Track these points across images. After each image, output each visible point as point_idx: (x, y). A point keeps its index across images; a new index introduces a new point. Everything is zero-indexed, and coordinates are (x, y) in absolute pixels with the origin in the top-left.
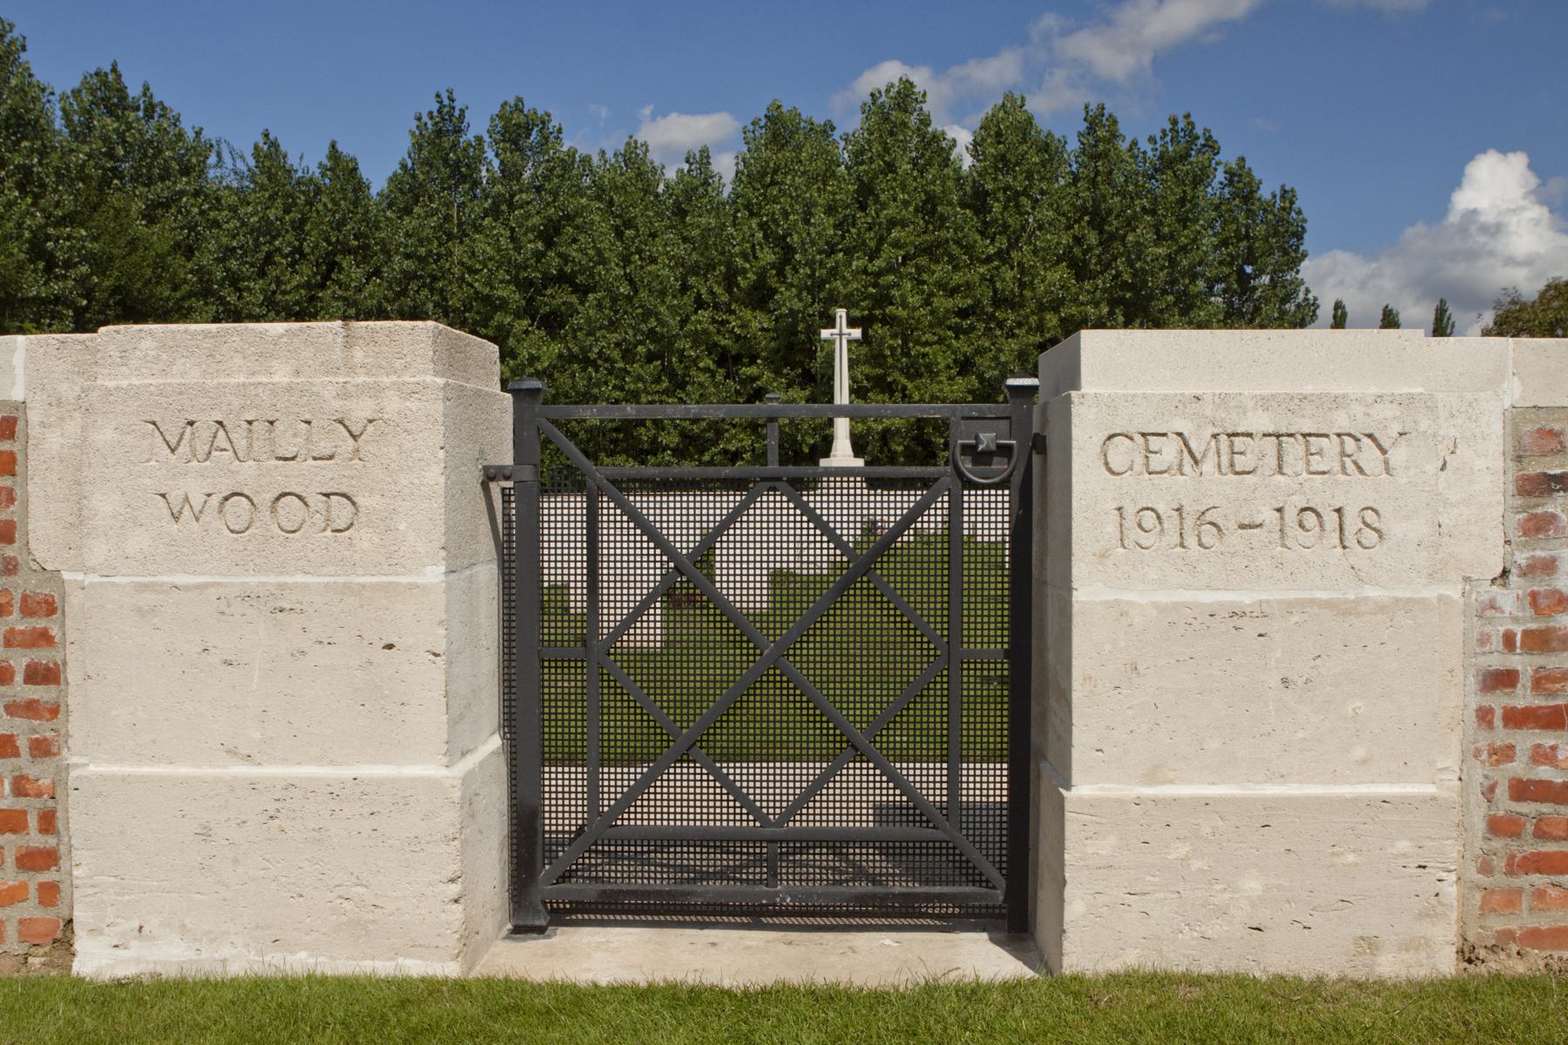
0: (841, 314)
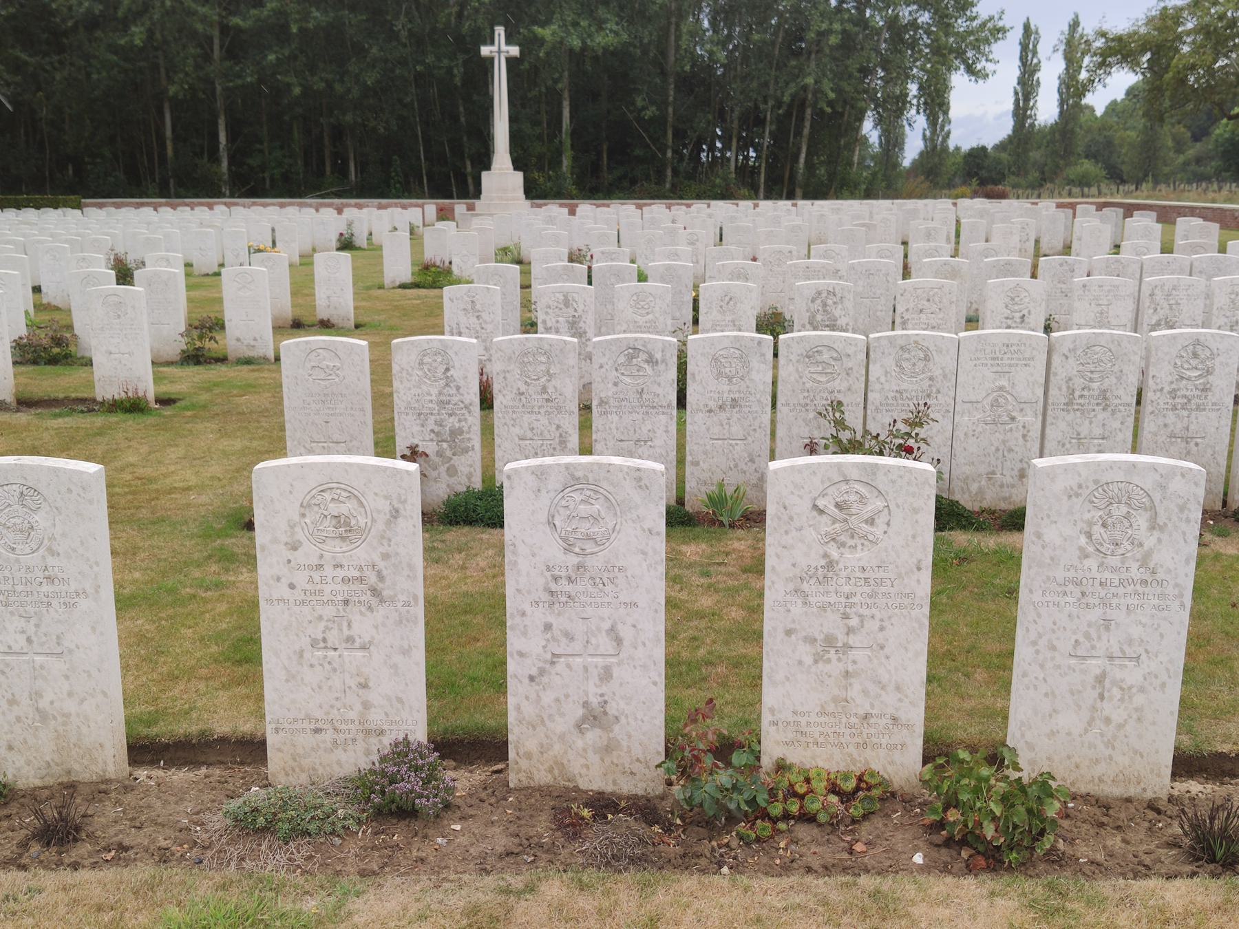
0: (500, 31)
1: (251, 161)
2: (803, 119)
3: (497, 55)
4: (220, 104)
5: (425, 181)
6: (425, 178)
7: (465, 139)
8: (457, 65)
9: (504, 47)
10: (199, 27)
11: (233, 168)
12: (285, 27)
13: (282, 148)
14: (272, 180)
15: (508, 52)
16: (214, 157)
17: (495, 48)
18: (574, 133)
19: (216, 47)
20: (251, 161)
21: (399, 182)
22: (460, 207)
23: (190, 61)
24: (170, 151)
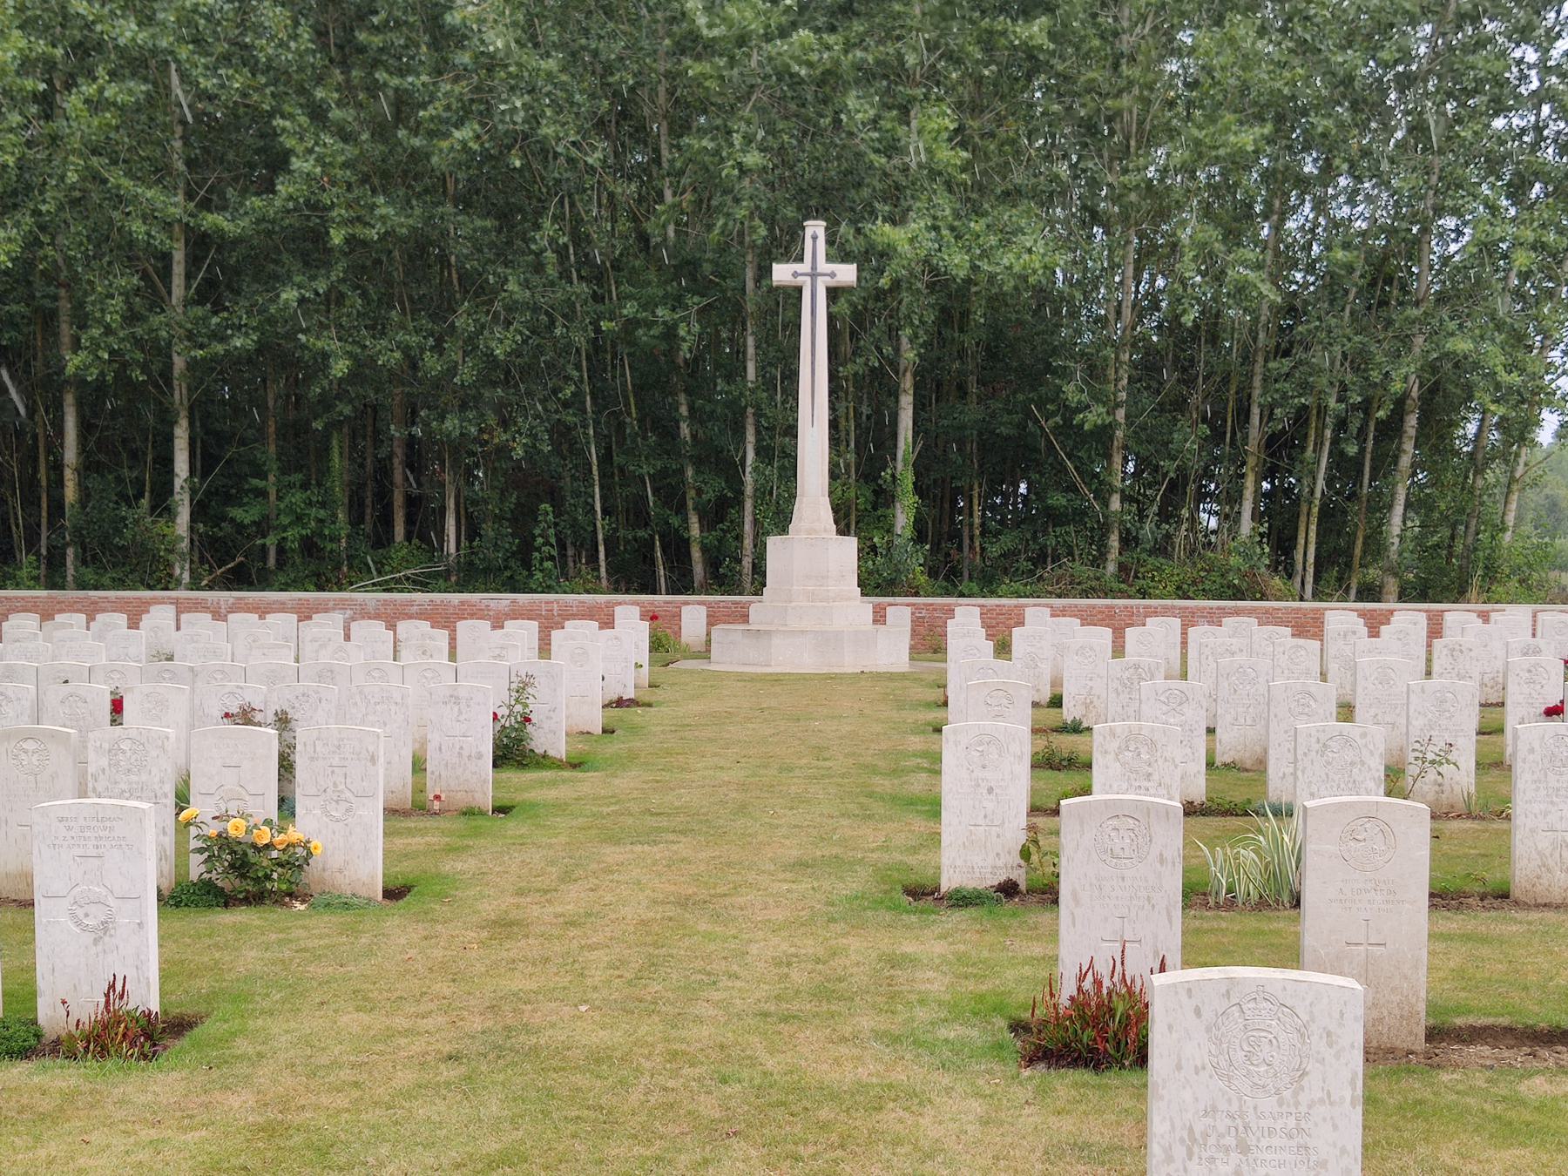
0: (815, 229)
1: (237, 513)
2: (1322, 443)
3: (808, 279)
4: (180, 395)
5: (602, 556)
6: (602, 549)
7: (690, 472)
8: (683, 319)
9: (823, 266)
10: (138, 228)
11: (201, 527)
12: (319, 237)
13: (305, 486)
14: (281, 550)
15: (833, 275)
16: (162, 506)
17: (805, 267)
18: (920, 468)
19: (178, 281)
20: (237, 513)
21: (552, 558)
22: (693, 614)
23: (117, 303)
24: (70, 493)
